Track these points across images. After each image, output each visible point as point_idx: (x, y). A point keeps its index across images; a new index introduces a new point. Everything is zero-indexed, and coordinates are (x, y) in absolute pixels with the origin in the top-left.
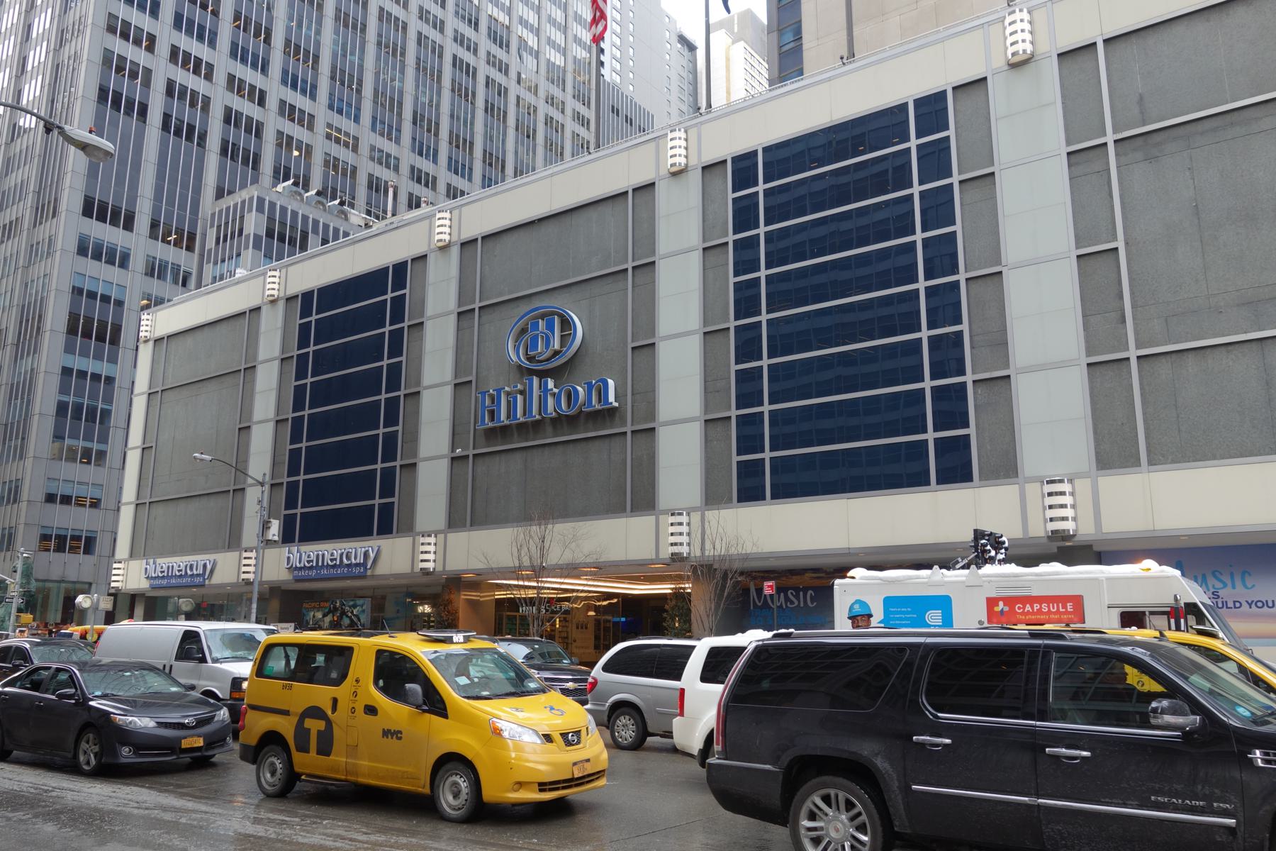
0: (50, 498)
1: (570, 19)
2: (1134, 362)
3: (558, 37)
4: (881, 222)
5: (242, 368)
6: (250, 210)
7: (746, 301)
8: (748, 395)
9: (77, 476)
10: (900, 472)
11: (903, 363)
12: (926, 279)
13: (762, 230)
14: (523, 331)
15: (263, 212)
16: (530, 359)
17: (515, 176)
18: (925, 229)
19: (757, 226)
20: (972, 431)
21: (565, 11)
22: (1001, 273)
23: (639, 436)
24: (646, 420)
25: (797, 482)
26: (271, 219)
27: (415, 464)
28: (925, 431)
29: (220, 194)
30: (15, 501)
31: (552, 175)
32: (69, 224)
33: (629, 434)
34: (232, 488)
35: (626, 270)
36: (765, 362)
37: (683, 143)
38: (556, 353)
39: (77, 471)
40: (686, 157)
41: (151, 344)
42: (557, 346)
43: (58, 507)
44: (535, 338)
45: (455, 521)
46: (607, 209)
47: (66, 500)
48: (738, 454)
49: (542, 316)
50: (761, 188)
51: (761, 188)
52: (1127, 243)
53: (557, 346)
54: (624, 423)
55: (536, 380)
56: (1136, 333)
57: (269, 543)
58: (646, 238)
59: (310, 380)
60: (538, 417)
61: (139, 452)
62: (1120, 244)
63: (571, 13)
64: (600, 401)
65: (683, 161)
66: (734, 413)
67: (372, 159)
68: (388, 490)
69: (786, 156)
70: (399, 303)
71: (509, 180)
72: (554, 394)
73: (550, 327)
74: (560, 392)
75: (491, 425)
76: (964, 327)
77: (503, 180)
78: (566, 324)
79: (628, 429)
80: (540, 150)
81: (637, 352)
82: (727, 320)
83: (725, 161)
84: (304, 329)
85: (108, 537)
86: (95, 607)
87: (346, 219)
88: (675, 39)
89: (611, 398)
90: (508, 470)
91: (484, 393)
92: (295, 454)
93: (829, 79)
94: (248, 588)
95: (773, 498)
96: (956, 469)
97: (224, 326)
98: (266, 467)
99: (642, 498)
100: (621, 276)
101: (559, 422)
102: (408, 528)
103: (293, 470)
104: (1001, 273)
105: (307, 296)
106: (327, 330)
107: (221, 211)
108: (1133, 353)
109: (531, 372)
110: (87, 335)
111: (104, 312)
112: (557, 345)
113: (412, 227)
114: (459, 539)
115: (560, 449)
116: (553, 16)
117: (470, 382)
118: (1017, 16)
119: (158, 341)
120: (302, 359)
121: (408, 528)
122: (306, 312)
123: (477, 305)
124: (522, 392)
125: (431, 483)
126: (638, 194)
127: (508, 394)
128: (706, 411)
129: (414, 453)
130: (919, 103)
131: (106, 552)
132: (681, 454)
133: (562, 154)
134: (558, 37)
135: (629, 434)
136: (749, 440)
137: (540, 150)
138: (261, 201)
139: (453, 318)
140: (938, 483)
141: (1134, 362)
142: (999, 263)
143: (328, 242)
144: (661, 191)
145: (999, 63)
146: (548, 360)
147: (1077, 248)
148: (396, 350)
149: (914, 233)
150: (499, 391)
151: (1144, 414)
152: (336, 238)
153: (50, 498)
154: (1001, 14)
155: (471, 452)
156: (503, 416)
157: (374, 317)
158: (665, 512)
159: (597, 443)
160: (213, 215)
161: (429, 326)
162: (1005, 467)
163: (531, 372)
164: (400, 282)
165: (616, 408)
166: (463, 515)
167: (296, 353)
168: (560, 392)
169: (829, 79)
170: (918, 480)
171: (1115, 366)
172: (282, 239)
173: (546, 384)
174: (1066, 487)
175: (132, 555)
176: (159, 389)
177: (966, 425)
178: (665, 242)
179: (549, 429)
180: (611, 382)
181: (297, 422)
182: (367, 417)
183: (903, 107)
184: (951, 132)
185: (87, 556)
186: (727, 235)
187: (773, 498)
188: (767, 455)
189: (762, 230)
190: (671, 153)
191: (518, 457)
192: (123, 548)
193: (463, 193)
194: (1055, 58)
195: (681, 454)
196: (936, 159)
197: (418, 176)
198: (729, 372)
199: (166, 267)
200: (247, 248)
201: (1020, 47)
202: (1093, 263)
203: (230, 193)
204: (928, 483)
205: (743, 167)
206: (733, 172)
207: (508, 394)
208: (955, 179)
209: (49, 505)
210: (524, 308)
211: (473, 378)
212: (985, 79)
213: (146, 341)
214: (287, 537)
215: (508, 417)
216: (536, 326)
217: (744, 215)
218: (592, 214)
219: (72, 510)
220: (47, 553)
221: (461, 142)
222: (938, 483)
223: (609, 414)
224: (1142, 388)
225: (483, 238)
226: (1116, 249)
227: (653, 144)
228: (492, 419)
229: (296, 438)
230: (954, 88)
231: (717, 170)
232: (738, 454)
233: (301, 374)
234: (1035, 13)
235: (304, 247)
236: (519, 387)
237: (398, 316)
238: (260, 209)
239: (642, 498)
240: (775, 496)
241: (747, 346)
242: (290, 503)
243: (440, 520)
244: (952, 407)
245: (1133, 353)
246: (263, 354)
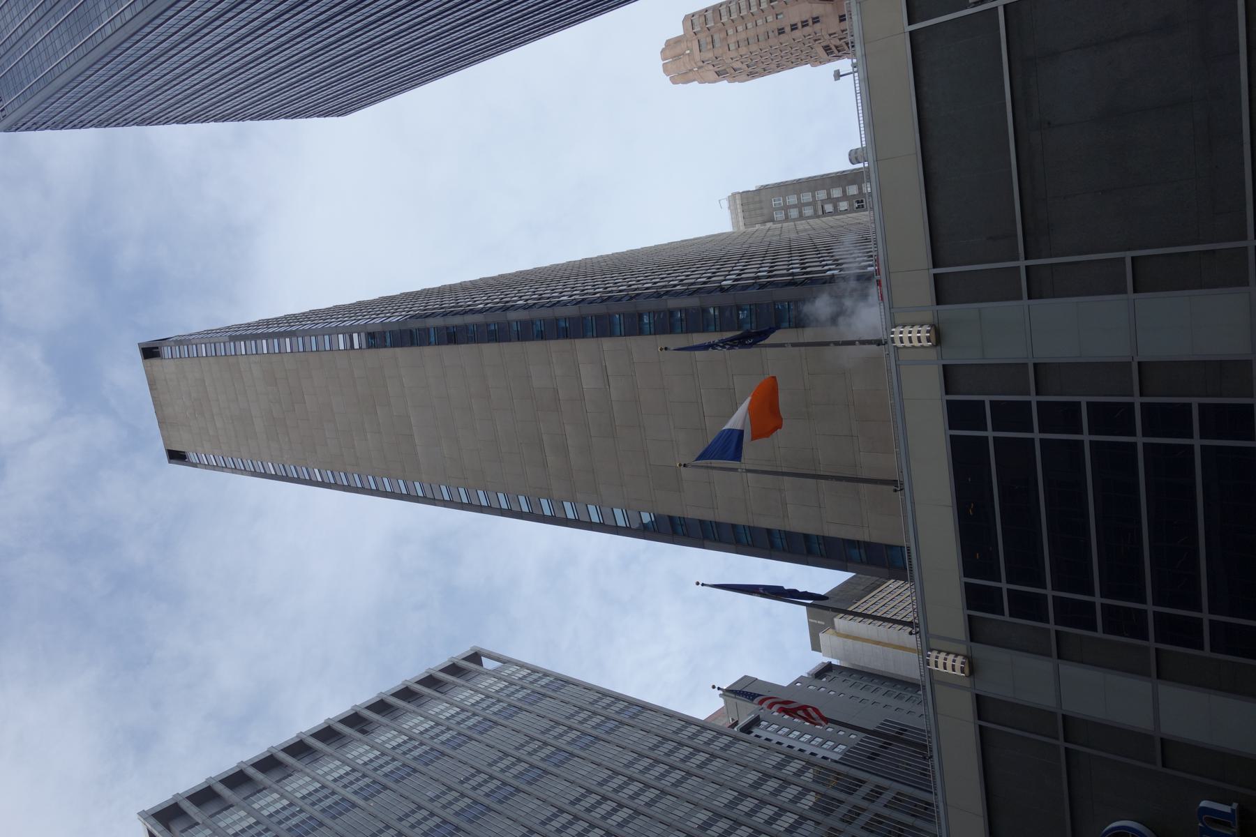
1: (778, 774)
3: (792, 791)
18: (1080, 432)
19: (1045, 596)
21: (770, 776)
22: (1139, 363)
28: (1192, 447)
31: (945, 804)
37: (943, 655)
40: (957, 655)
52: (1129, 249)
65: (959, 659)
80: (919, 823)
88: (818, 682)
93: (913, 503)
104: (1139, 363)
116: (771, 789)
118: (897, 336)
125: (1060, 628)
133: (927, 803)
134: (792, 791)
137: (919, 823)
142: (1128, 365)
144: (990, 689)
145: (933, 354)
147: (1126, 292)
154: (892, 350)
169: (913, 503)
178: (1045, 700)
180: (1203, 804)
183: (968, 587)
184: (987, 399)
186: (1048, 630)
190: (949, 670)
194: (973, 644)
196: (1012, 415)
201: (924, 335)
202: (1146, 278)
204: (951, 428)
205: (976, 598)
212: (978, 696)
217: (1028, 607)
225: (980, 717)
226: (1133, 258)
227: (937, 687)
234: (897, 322)
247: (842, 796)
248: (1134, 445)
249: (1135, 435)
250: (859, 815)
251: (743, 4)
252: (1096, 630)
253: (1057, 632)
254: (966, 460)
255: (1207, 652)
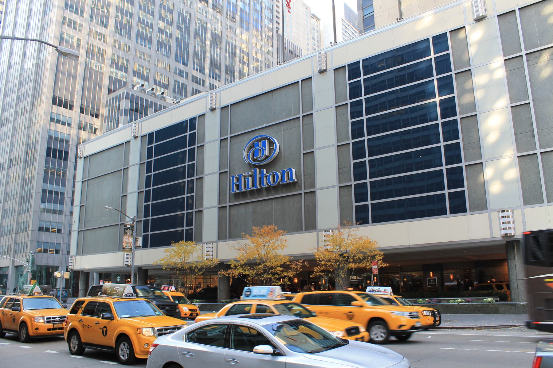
0: (41, 229)
2: (539, 155)
4: (413, 94)
5: (122, 169)
6: (123, 98)
7: (357, 131)
8: (359, 173)
9: (51, 219)
10: (433, 209)
11: (432, 158)
12: (368, 135)
13: (363, 97)
14: (251, 147)
15: (128, 99)
16: (255, 160)
17: (240, 78)
20: (465, 189)
23: (308, 195)
24: (311, 187)
25: (384, 215)
26: (132, 102)
27: (202, 211)
29: (110, 91)
30: (26, 231)
32: (44, 106)
33: (303, 194)
34: (119, 223)
35: (227, 138)
36: (367, 159)
38: (267, 157)
39: (50, 217)
41: (83, 159)
42: (267, 154)
43: (44, 233)
44: (256, 151)
45: (221, 237)
46: (289, 89)
47: (47, 230)
48: (356, 202)
49: (260, 140)
50: (362, 78)
51: (362, 78)
52: (533, 101)
53: (267, 154)
54: (300, 189)
55: (258, 170)
56: (540, 142)
57: (137, 248)
58: (308, 103)
59: (153, 173)
60: (259, 187)
61: (79, 207)
62: (531, 101)
63: (263, 5)
64: (288, 179)
66: (353, 183)
67: (176, 73)
68: (190, 223)
69: (371, 64)
70: (193, 136)
71: (237, 80)
72: (266, 177)
73: (264, 145)
74: (270, 175)
75: (237, 191)
76: (460, 140)
77: (234, 81)
78: (271, 143)
79: (302, 192)
81: (305, 155)
82: (348, 139)
83: (345, 66)
84: (150, 150)
85: (65, 246)
86: (62, 277)
87: (165, 100)
89: (294, 178)
90: (245, 212)
91: (233, 177)
92: (147, 207)
94: (129, 269)
95: (373, 222)
96: (459, 206)
97: (114, 149)
98: (135, 214)
99: (310, 224)
100: (297, 120)
101: (269, 189)
102: (199, 240)
103: (146, 215)
105: (151, 135)
106: (160, 150)
107: (110, 100)
108: (538, 151)
109: (256, 166)
110: (54, 156)
111: (55, 144)
112: (267, 153)
113: (198, 101)
114: (223, 245)
115: (270, 202)
117: (227, 172)
119: (86, 158)
120: (149, 164)
121: (199, 240)
122: (150, 142)
123: (229, 136)
124: (251, 176)
126: (304, 82)
127: (245, 177)
128: (340, 182)
129: (201, 205)
130: (434, 38)
131: (65, 252)
132: (328, 203)
135: (303, 194)
136: (360, 196)
138: (127, 94)
139: (218, 142)
140: (451, 213)
141: (539, 155)
143: (157, 111)
144: (215, 238)
146: (263, 160)
148: (192, 158)
149: (362, 116)
150: (240, 176)
151: (545, 179)
152: (160, 109)
153: (41, 229)
155: (228, 204)
156: (243, 187)
157: (181, 143)
158: (321, 230)
159: (287, 199)
160: (107, 101)
161: (206, 147)
162: (481, 205)
163: (256, 166)
164: (193, 127)
165: (296, 182)
166: (226, 232)
167: (146, 161)
168: (270, 175)
169: (392, 29)
170: (442, 212)
171: (530, 157)
172: (136, 111)
173: (263, 171)
174: (510, 213)
175: (221, 237)
176: (86, 179)
177: (463, 186)
178: (317, 105)
179: (265, 193)
180: (294, 170)
181: (147, 193)
182: (179, 189)
185: (57, 255)
186: (347, 100)
187: (373, 222)
188: (369, 202)
189: (363, 97)
191: (250, 206)
192: (73, 251)
193: (199, 92)
195: (328, 203)
197: (196, 80)
198: (350, 164)
199: (87, 125)
200: (121, 115)
203: (114, 91)
205: (353, 69)
206: (349, 71)
207: (245, 177)
208: (453, 73)
209: (40, 232)
210: (251, 136)
211: (228, 170)
213: (81, 158)
214: (145, 245)
215: (245, 188)
216: (257, 145)
217: (355, 91)
218: (283, 92)
219: (48, 234)
220: (40, 253)
221: (215, 64)
222: (451, 213)
223: (293, 185)
224: (543, 167)
228: (238, 189)
229: (147, 200)
230: (519, 9)
231: (341, 70)
232: (356, 202)
233: (149, 171)
235: (146, 114)
236: (250, 173)
237: (192, 142)
238: (127, 98)
239: (310, 224)
240: (373, 222)
241: (358, 152)
242: (146, 230)
243: (215, 237)
244: (456, 178)
245: (538, 151)
246: (131, 162)
247: (207, 71)
248: (439, 142)
249: (448, 189)
250: (200, 84)
251: (37, 7)
252: (351, 119)
253: (347, 104)
254: (415, 50)
255: (352, 162)
